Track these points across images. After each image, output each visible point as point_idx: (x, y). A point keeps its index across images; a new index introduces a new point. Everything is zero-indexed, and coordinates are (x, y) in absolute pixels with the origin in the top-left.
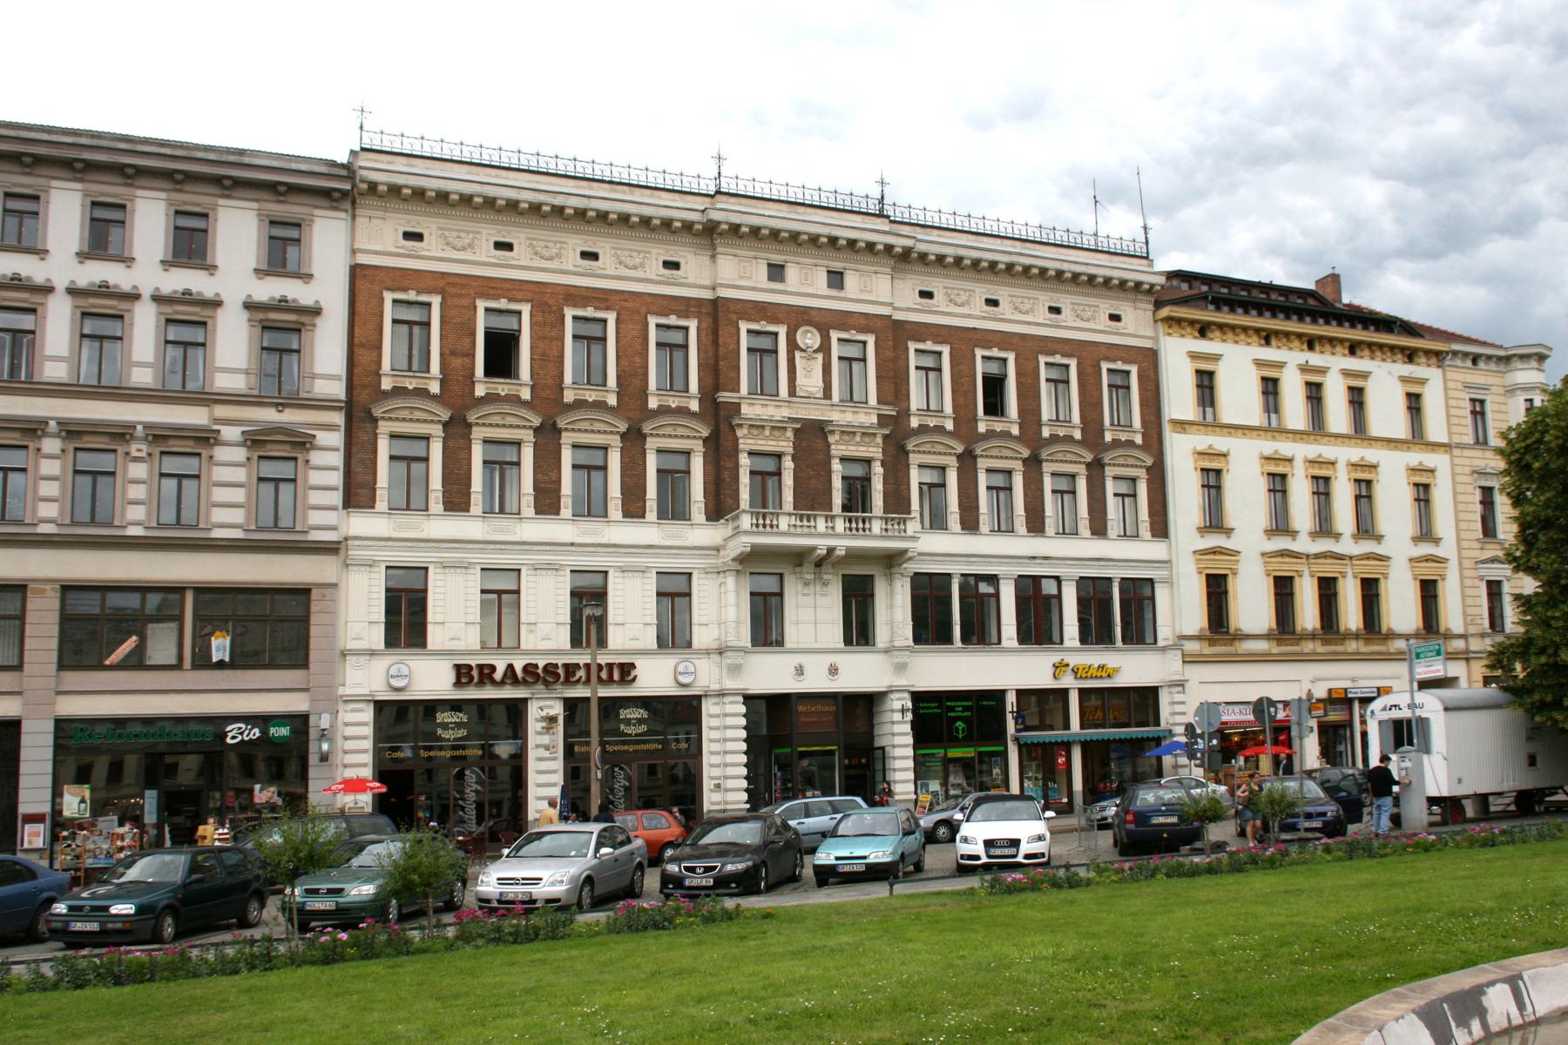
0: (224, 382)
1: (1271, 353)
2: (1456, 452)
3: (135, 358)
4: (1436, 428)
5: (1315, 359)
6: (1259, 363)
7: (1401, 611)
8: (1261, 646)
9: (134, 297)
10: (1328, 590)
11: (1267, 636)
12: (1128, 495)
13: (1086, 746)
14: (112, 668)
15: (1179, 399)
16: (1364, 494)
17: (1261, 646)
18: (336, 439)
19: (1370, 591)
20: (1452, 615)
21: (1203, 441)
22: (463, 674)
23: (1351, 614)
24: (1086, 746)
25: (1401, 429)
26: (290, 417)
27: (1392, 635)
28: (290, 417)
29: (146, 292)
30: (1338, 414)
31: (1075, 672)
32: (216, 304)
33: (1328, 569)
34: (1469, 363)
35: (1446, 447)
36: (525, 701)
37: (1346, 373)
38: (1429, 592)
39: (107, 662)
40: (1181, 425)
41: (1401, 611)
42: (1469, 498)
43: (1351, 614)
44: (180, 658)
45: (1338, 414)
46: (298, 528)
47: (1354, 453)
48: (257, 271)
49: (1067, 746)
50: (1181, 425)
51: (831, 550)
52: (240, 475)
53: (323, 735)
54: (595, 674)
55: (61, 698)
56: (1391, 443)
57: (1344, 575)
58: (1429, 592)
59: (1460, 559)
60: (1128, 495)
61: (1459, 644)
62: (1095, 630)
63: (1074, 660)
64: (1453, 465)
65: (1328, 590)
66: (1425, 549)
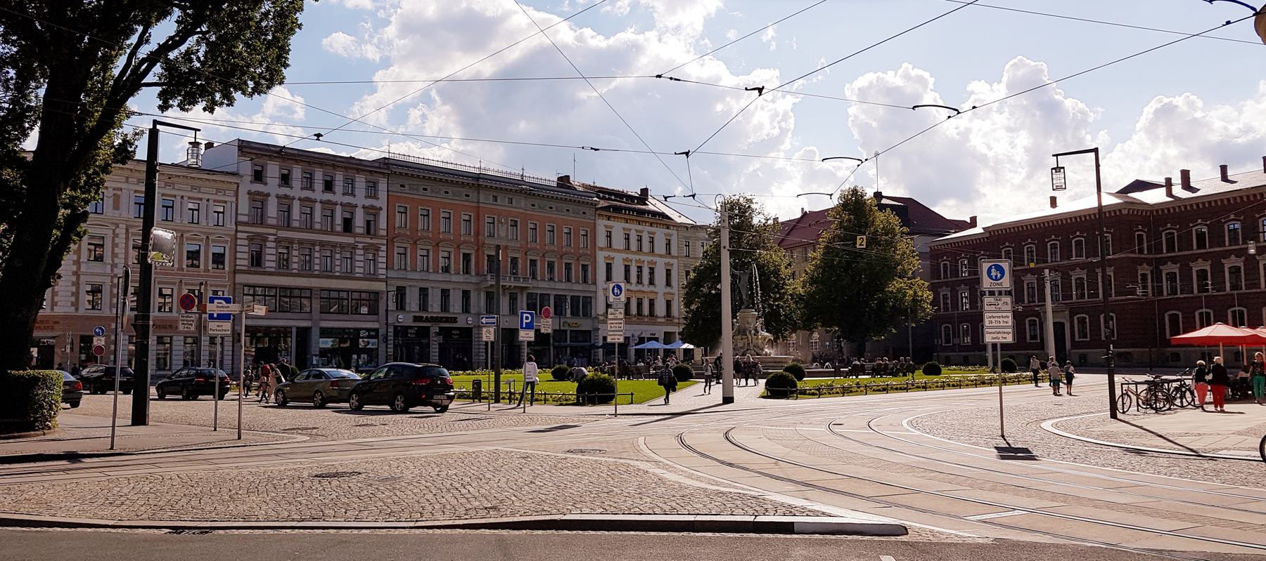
0: (270, 221)
1: (627, 226)
2: (680, 259)
3: (357, 225)
4: (674, 251)
5: (640, 228)
6: (624, 229)
7: (660, 310)
8: (663, 320)
9: (293, 198)
10: (640, 304)
11: (664, 317)
12: (403, 254)
13: (572, 348)
14: (332, 313)
15: (601, 241)
16: (652, 271)
17: (663, 320)
18: (384, 248)
19: (652, 303)
20: (675, 312)
21: (607, 253)
22: (416, 319)
23: (646, 311)
24: (572, 348)
25: (663, 252)
26: (374, 241)
27: (657, 317)
28: (374, 241)
29: (297, 197)
30: (646, 246)
31: (569, 325)
32: (268, 195)
33: (640, 296)
34: (685, 229)
35: (677, 257)
36: (429, 327)
37: (649, 233)
38: (669, 304)
39: (332, 310)
40: (601, 249)
41: (660, 310)
42: (683, 274)
43: (646, 311)
44: (276, 308)
45: (646, 246)
46: (333, 271)
47: (650, 258)
48: (279, 185)
49: (566, 347)
50: (601, 249)
51: (510, 286)
52: (274, 251)
53: (685, 318)
54: (448, 320)
55: (322, 322)
56: (661, 256)
57: (632, 296)
58: (669, 304)
59: (679, 294)
60: (403, 254)
61: (677, 321)
62: (575, 313)
63: (568, 321)
64: (678, 263)
65: (640, 304)
66: (668, 289)
